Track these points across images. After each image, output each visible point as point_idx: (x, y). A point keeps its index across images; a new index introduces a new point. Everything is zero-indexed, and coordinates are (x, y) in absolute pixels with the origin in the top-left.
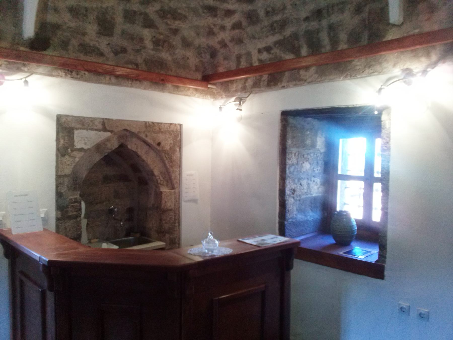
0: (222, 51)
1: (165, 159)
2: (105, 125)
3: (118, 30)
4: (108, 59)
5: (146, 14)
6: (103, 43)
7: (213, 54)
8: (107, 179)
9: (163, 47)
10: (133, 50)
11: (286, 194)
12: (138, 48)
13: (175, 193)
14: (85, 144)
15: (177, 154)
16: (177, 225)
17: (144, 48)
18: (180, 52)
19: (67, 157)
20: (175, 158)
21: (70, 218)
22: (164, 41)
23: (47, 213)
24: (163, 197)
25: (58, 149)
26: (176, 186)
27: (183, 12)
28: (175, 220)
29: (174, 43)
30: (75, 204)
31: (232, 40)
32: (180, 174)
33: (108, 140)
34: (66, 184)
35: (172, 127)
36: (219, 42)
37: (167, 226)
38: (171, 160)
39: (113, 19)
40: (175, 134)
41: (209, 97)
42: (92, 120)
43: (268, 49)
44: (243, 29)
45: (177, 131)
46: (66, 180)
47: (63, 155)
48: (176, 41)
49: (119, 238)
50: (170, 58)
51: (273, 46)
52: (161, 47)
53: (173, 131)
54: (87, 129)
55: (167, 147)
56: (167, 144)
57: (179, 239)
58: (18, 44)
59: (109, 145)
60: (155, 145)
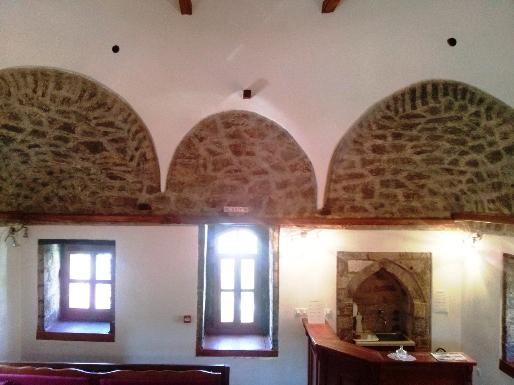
0: (464, 196)
1: (417, 279)
2: (369, 256)
3: (377, 193)
4: (370, 213)
5: (397, 180)
6: (367, 204)
7: (457, 199)
8: (377, 289)
9: (413, 198)
10: (389, 204)
11: (507, 322)
12: (393, 202)
13: (426, 305)
14: (355, 269)
15: (428, 275)
16: (428, 330)
17: (398, 201)
18: (428, 200)
19: (343, 277)
20: (426, 278)
21: (346, 316)
22: (414, 194)
23: (331, 311)
24: (415, 308)
25: (338, 272)
26: (427, 300)
27: (427, 174)
28: (426, 326)
29: (423, 194)
30: (349, 307)
31: (469, 190)
32: (431, 291)
33: (372, 265)
34: (343, 293)
35: (423, 256)
36: (460, 191)
37: (419, 330)
38: (423, 280)
39: (373, 187)
40: (426, 261)
41: (458, 229)
42: (360, 254)
43: (493, 201)
44: (475, 184)
45: (427, 258)
46: (343, 291)
47: (341, 276)
48: (425, 192)
49: (386, 332)
50: (420, 205)
51: (496, 200)
52: (411, 199)
53: (423, 258)
54: (356, 260)
55: (419, 271)
56: (418, 267)
57: (430, 341)
58: (314, 213)
59: (373, 269)
60: (407, 269)
